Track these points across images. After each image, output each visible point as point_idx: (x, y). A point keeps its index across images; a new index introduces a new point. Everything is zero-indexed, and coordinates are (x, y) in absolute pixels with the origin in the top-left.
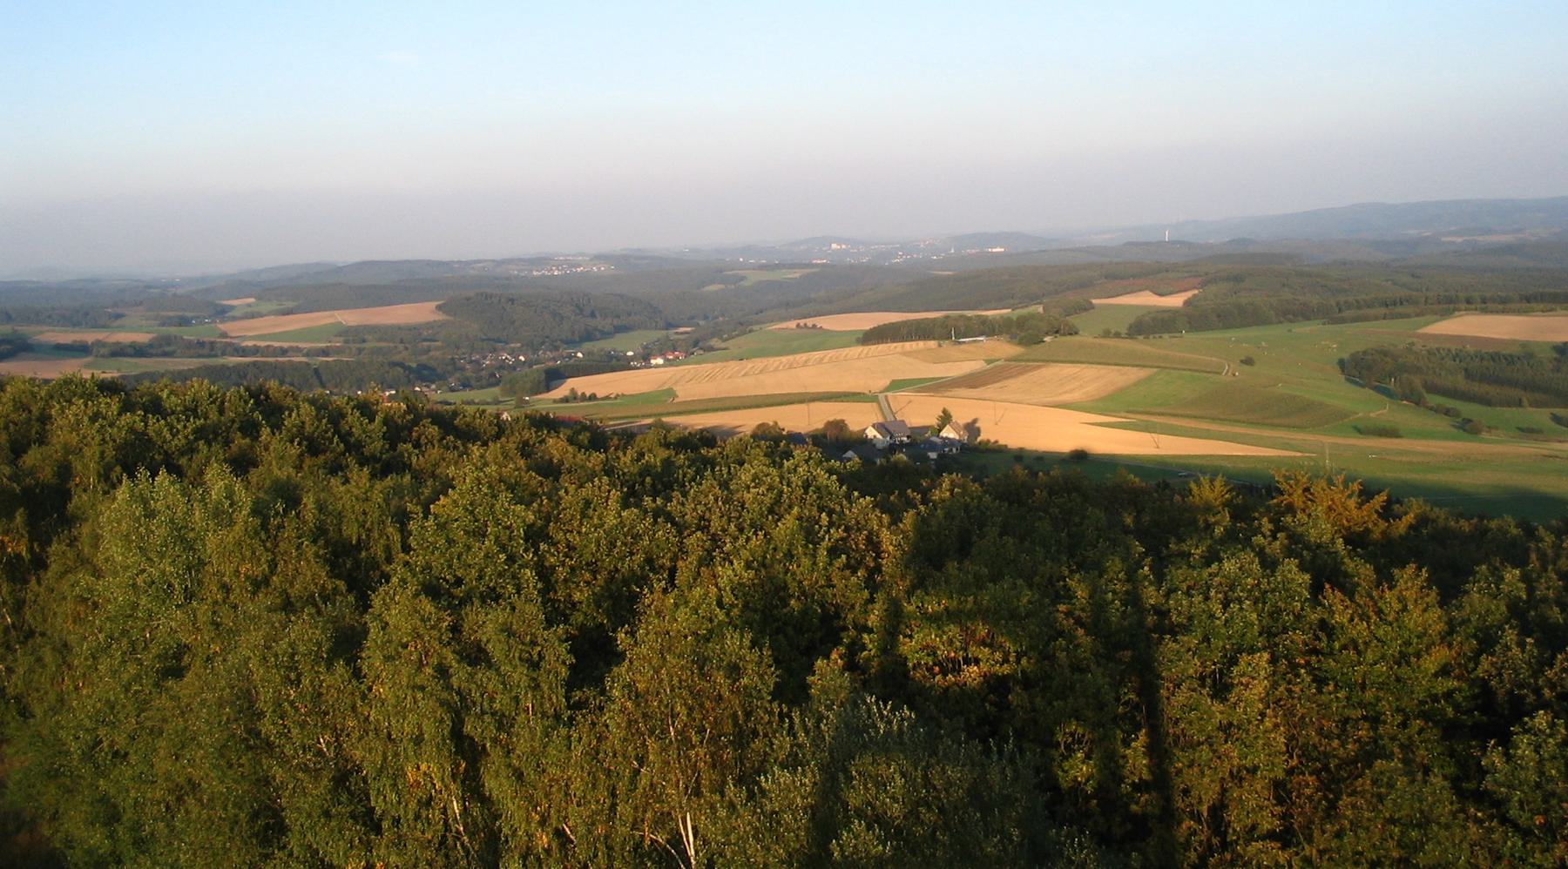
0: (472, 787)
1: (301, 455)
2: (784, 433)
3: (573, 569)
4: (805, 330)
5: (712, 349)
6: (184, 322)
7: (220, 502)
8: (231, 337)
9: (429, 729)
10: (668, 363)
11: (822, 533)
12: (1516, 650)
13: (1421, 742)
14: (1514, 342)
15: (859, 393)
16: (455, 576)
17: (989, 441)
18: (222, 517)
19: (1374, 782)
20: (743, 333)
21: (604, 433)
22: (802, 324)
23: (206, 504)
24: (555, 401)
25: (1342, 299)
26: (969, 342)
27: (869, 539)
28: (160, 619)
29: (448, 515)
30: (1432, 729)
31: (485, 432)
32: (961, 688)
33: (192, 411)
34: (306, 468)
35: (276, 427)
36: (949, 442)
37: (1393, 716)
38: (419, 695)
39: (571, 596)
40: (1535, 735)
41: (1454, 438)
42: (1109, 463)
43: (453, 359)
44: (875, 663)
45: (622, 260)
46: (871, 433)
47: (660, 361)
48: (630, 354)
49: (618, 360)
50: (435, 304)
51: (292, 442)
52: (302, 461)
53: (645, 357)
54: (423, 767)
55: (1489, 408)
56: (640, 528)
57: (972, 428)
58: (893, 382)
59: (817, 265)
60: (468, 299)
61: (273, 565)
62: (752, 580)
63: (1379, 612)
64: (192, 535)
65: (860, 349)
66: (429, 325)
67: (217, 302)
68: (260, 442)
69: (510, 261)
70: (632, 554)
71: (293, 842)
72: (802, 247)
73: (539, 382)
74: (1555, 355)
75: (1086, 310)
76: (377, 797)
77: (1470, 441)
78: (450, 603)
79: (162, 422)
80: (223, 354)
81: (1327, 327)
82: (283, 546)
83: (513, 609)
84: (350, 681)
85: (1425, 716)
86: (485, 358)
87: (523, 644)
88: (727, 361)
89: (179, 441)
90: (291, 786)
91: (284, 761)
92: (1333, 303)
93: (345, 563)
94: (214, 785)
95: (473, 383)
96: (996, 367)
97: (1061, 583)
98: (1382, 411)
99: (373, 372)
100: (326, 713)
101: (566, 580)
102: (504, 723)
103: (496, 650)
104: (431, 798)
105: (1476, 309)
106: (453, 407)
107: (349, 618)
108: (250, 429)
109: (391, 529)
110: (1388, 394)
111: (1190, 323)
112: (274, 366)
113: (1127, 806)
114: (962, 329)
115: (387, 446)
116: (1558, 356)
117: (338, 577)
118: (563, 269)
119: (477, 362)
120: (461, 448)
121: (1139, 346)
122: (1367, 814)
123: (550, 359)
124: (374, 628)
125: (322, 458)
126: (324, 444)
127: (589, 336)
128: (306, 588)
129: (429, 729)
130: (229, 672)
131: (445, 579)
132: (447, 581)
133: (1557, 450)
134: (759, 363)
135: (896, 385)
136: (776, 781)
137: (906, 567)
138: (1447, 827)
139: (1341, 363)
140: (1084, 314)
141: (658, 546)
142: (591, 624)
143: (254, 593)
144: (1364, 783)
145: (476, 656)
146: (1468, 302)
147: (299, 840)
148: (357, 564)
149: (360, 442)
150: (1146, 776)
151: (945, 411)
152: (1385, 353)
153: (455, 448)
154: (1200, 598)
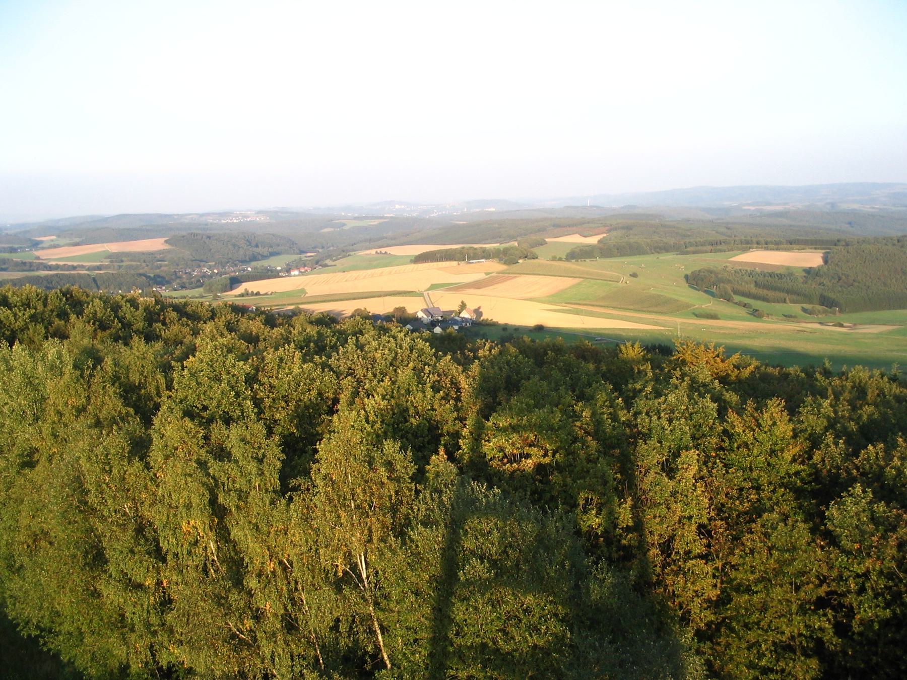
0: (223, 534)
1: (95, 330)
2: (370, 314)
3: (274, 400)
4: (385, 255)
5: (326, 266)
6: (13, 250)
7: (54, 361)
8: (42, 260)
9: (195, 500)
10: (302, 274)
11: (425, 377)
12: (833, 446)
13: (783, 501)
14: (782, 266)
15: (413, 292)
16: (202, 405)
17: (487, 319)
18: (55, 370)
19: (763, 526)
20: (344, 257)
21: (273, 315)
22: (379, 252)
23: (45, 362)
24: (236, 296)
25: (687, 240)
26: (476, 262)
27: (452, 383)
28: (18, 433)
29: (197, 368)
30: (789, 493)
31: (204, 316)
32: (521, 472)
33: (27, 305)
34: (99, 338)
35: (79, 313)
36: (465, 320)
37: (768, 486)
38: (189, 479)
39: (273, 416)
40: (855, 498)
41: (750, 320)
42: (555, 332)
43: (175, 271)
44: (466, 457)
45: (274, 214)
46: (420, 315)
47: (296, 272)
48: (279, 268)
49: (272, 272)
50: (163, 240)
51: (89, 322)
52: (96, 335)
53: (288, 270)
54: (192, 522)
55: (768, 304)
56: (314, 375)
57: (478, 312)
58: (432, 285)
59: (387, 218)
60: (183, 237)
61: (88, 398)
62: (386, 406)
63: (759, 426)
64: (37, 381)
65: (413, 266)
66: (161, 252)
67: (34, 238)
68: (71, 323)
69: (208, 214)
70: (309, 390)
71: (112, 568)
72: (378, 207)
73: (226, 285)
74: (805, 274)
75: (542, 245)
76: (164, 541)
77: (757, 322)
78: (200, 421)
79: (9, 311)
80: (38, 269)
81: (679, 256)
82: (94, 388)
83: (247, 427)
84: (143, 471)
85: (785, 486)
86: (194, 271)
87: (254, 448)
88: (335, 272)
89: (20, 323)
90: (108, 535)
91: (103, 519)
92: (682, 243)
93: (132, 397)
94: (58, 532)
95: (187, 285)
96: (491, 277)
97: (571, 408)
98: (708, 304)
99: (128, 280)
100: (128, 490)
101: (270, 406)
102: (242, 495)
103: (236, 453)
104: (197, 542)
105: (762, 248)
106: (184, 300)
107: (140, 431)
108: (63, 315)
109: (159, 376)
110: (712, 294)
111: (601, 253)
112: (69, 276)
113: (619, 541)
114: (472, 255)
115: (146, 325)
116: (806, 275)
117: (128, 405)
118: (239, 219)
119: (190, 273)
120: (191, 325)
121: (572, 265)
122: (759, 545)
123: (232, 271)
124: (155, 437)
125: (108, 332)
126: (109, 324)
127: (254, 258)
128: (109, 413)
129: (195, 500)
130: (67, 466)
131: (196, 407)
132: (198, 408)
133: (805, 328)
134: (354, 274)
135: (433, 287)
136: (418, 534)
137: (476, 398)
138: (805, 552)
139: (686, 277)
140: (541, 247)
141: (325, 385)
142: (286, 433)
143: (77, 417)
144: (756, 526)
145: (222, 454)
146: (758, 243)
147: (116, 568)
148: (139, 398)
149: (130, 322)
150: (631, 524)
151: (462, 302)
152: (711, 272)
153: (188, 325)
154: (656, 417)
